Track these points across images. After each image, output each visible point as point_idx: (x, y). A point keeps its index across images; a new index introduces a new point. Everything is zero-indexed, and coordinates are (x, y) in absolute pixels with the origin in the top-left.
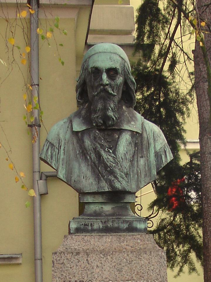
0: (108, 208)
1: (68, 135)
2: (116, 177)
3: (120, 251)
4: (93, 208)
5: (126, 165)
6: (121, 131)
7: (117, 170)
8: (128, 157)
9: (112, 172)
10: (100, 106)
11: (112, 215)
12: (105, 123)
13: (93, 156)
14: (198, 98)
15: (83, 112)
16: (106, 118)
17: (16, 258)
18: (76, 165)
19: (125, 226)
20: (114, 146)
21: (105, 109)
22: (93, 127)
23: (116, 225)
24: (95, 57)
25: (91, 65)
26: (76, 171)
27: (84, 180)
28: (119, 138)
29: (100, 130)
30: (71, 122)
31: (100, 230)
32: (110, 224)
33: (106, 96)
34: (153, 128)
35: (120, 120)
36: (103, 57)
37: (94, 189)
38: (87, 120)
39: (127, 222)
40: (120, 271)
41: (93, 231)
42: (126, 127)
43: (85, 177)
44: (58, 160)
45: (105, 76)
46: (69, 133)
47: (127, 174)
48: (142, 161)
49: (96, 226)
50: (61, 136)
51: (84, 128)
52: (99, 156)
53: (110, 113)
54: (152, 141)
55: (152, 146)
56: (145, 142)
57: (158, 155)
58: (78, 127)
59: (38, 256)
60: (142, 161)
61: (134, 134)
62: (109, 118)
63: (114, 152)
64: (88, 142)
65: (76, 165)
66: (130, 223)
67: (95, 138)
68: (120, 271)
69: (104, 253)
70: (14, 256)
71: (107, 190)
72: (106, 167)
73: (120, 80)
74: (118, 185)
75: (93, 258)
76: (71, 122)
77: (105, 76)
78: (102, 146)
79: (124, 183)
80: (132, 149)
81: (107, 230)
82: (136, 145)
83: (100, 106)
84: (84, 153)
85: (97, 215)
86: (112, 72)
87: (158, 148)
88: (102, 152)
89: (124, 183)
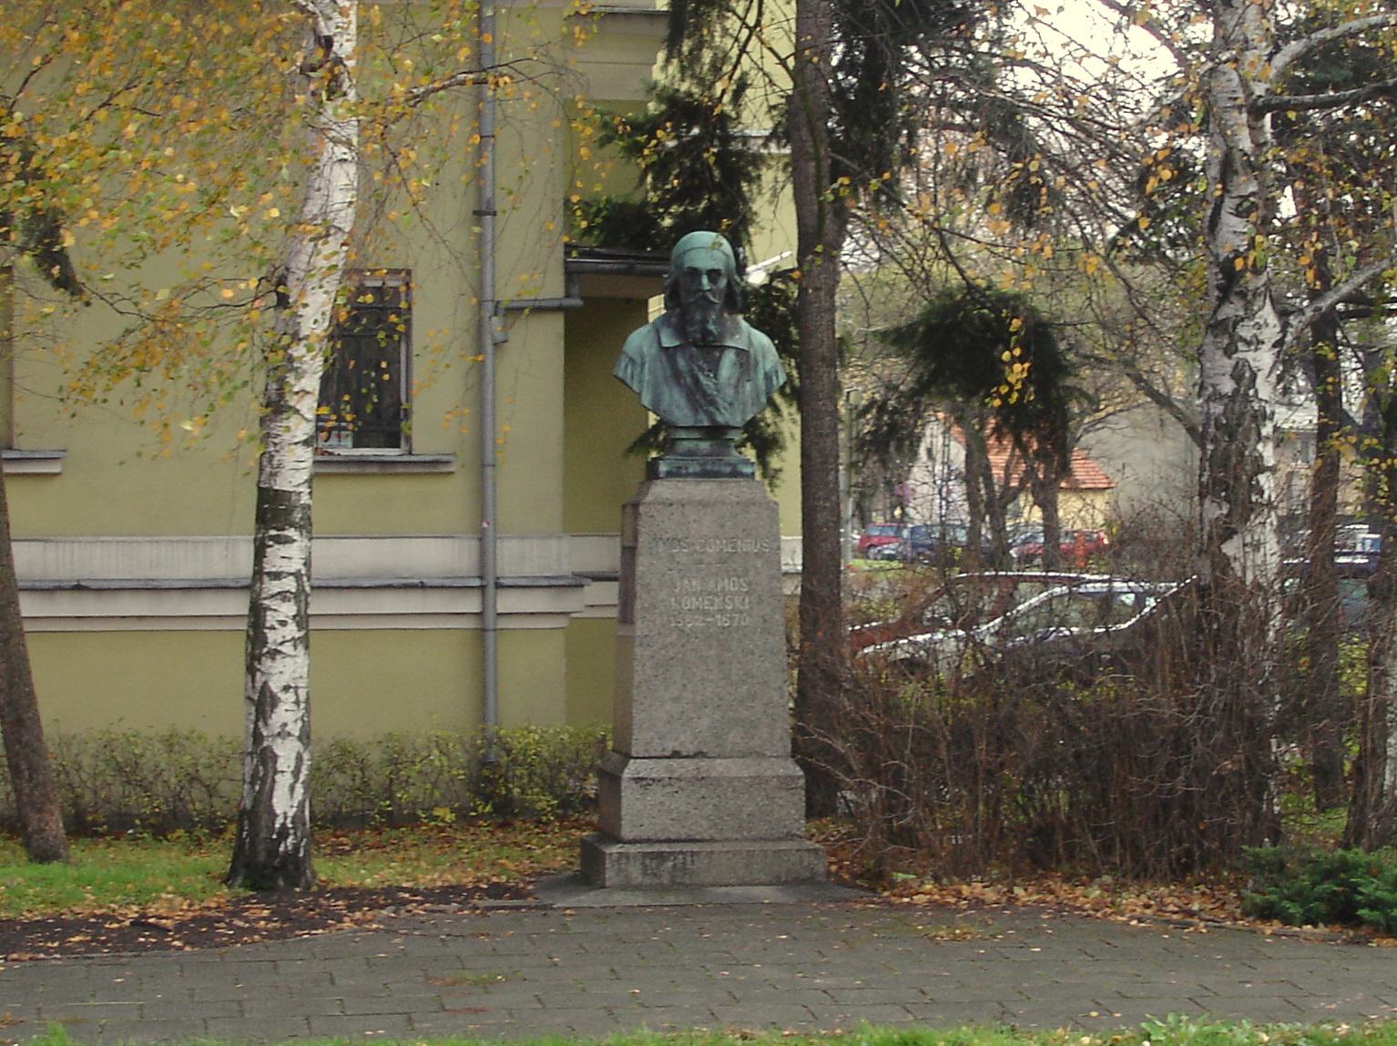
0: (705, 446)
1: (654, 350)
2: (718, 409)
3: (723, 503)
4: (686, 445)
5: (730, 392)
6: (724, 348)
7: (718, 399)
8: (733, 381)
9: (713, 403)
10: (698, 317)
11: (710, 455)
12: (704, 338)
13: (689, 380)
14: (807, 444)
15: (674, 320)
16: (706, 333)
17: (447, 463)
18: (665, 389)
19: (728, 469)
20: (715, 368)
21: (705, 321)
22: (689, 343)
23: (716, 468)
24: (692, 254)
25: (687, 265)
26: (666, 397)
27: (676, 411)
28: (720, 357)
29: (697, 346)
30: (658, 333)
31: (696, 475)
32: (709, 467)
33: (706, 304)
34: (761, 339)
35: (721, 336)
36: (703, 254)
37: (690, 423)
38: (680, 331)
39: (730, 465)
40: (722, 526)
41: (688, 475)
42: (729, 343)
43: (678, 407)
44: (641, 382)
45: (705, 280)
46: (655, 347)
47: (731, 404)
48: (748, 386)
49: (691, 470)
50: (645, 349)
51: (677, 343)
52: (696, 381)
53: (711, 327)
54: (760, 358)
55: (761, 365)
56: (752, 361)
57: (768, 377)
58: (668, 341)
59: (489, 459)
60: (748, 386)
61: (739, 352)
62: (710, 332)
63: (715, 377)
64: (682, 363)
65: (665, 389)
66: (734, 466)
67: (692, 356)
68: (722, 526)
69: (703, 504)
70: (445, 458)
71: (706, 424)
72: (705, 394)
73: (723, 283)
74: (720, 419)
75: (688, 510)
76: (658, 333)
77: (705, 280)
78: (702, 370)
79: (727, 416)
80: (737, 371)
81: (705, 474)
82: (741, 365)
83: (698, 317)
84: (677, 375)
85: (691, 454)
86: (713, 274)
87: (768, 367)
88: (702, 378)
89: (727, 416)
